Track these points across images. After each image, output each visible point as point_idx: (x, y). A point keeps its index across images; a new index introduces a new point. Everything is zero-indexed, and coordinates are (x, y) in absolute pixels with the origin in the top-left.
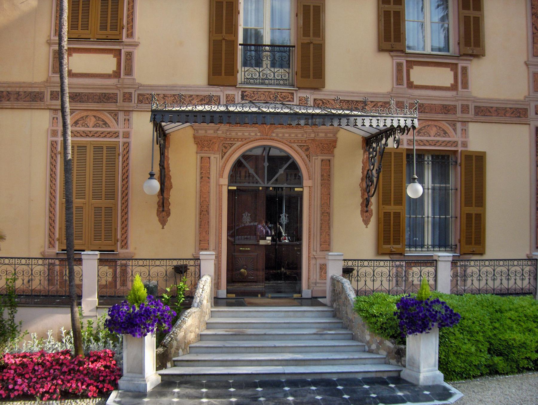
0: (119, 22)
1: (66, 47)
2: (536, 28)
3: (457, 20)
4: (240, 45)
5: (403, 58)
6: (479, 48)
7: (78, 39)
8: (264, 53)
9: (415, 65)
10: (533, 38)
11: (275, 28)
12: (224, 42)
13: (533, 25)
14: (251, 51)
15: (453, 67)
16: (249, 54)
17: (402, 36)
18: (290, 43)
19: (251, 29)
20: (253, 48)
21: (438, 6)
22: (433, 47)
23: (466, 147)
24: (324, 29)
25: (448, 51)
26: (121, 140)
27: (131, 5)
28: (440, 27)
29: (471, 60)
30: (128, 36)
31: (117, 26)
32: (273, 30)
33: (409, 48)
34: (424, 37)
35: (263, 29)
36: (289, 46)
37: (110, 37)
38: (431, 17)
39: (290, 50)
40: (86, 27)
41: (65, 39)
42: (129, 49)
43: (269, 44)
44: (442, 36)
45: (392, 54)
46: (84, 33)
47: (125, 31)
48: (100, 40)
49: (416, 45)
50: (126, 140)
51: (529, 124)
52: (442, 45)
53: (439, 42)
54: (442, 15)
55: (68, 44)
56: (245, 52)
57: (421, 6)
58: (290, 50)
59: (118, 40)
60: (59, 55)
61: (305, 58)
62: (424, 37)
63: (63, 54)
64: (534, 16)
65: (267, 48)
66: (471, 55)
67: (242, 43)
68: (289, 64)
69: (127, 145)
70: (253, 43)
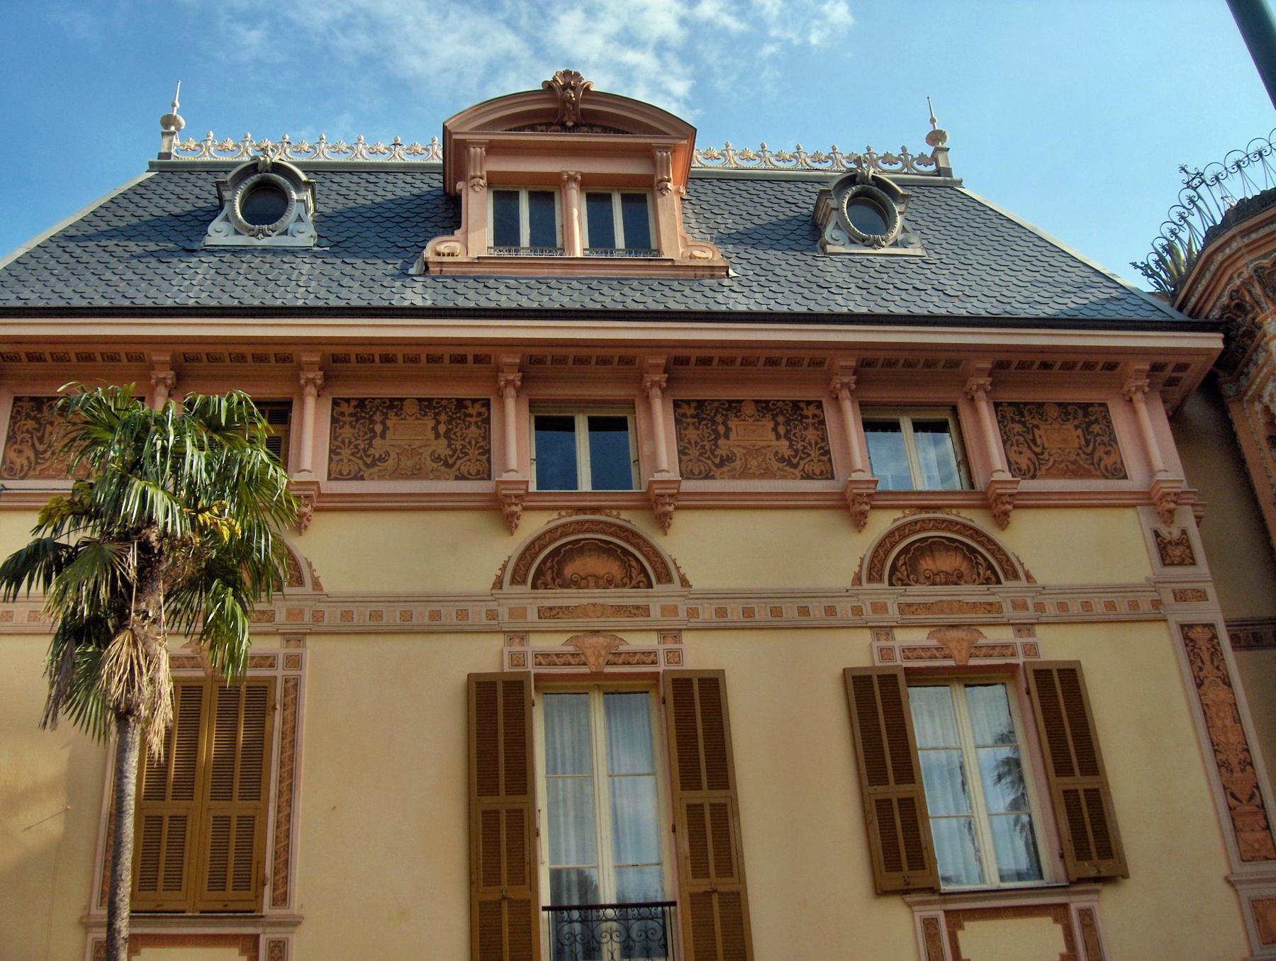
0: (254, 869)
1: (125, 933)
2: (1233, 795)
3: (1048, 805)
4: (545, 909)
5: (936, 907)
6: (1111, 862)
7: (156, 914)
8: (604, 926)
9: (969, 919)
10: (1233, 819)
11: (623, 863)
12: (505, 905)
13: (1225, 788)
14: (571, 921)
15: (1059, 912)
16: (566, 929)
17: (925, 854)
18: (664, 896)
19: (568, 870)
20: (575, 914)
21: (1000, 778)
22: (1005, 873)
23: (1036, 654)
24: (740, 854)
25: (1041, 876)
26: (280, 672)
27: (284, 828)
28: (1012, 823)
29: (1097, 892)
30: (275, 902)
31: (249, 879)
32: (620, 869)
33: (947, 880)
34: (977, 851)
35: (597, 867)
36: (663, 904)
37: (232, 907)
38: (987, 805)
39: (663, 913)
40: (175, 883)
41: (125, 912)
42: (277, 933)
43: (614, 902)
44: (1020, 844)
45: (908, 898)
46: (171, 899)
47: (268, 891)
48: (208, 914)
49: (963, 872)
50: (292, 673)
51: (1165, 621)
52: (1024, 864)
53: (1015, 859)
54: (1012, 797)
55: (131, 925)
56: (557, 924)
57: (959, 780)
58: (663, 913)
59: (250, 913)
60: (107, 951)
61: (702, 927)
62: (977, 851)
63: (117, 949)
64: (1223, 770)
65: (610, 912)
66: (1096, 880)
67: (548, 904)
68: (665, 945)
69: (294, 686)
70: (576, 902)
